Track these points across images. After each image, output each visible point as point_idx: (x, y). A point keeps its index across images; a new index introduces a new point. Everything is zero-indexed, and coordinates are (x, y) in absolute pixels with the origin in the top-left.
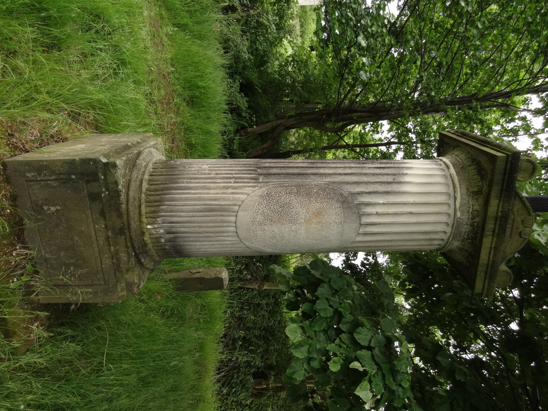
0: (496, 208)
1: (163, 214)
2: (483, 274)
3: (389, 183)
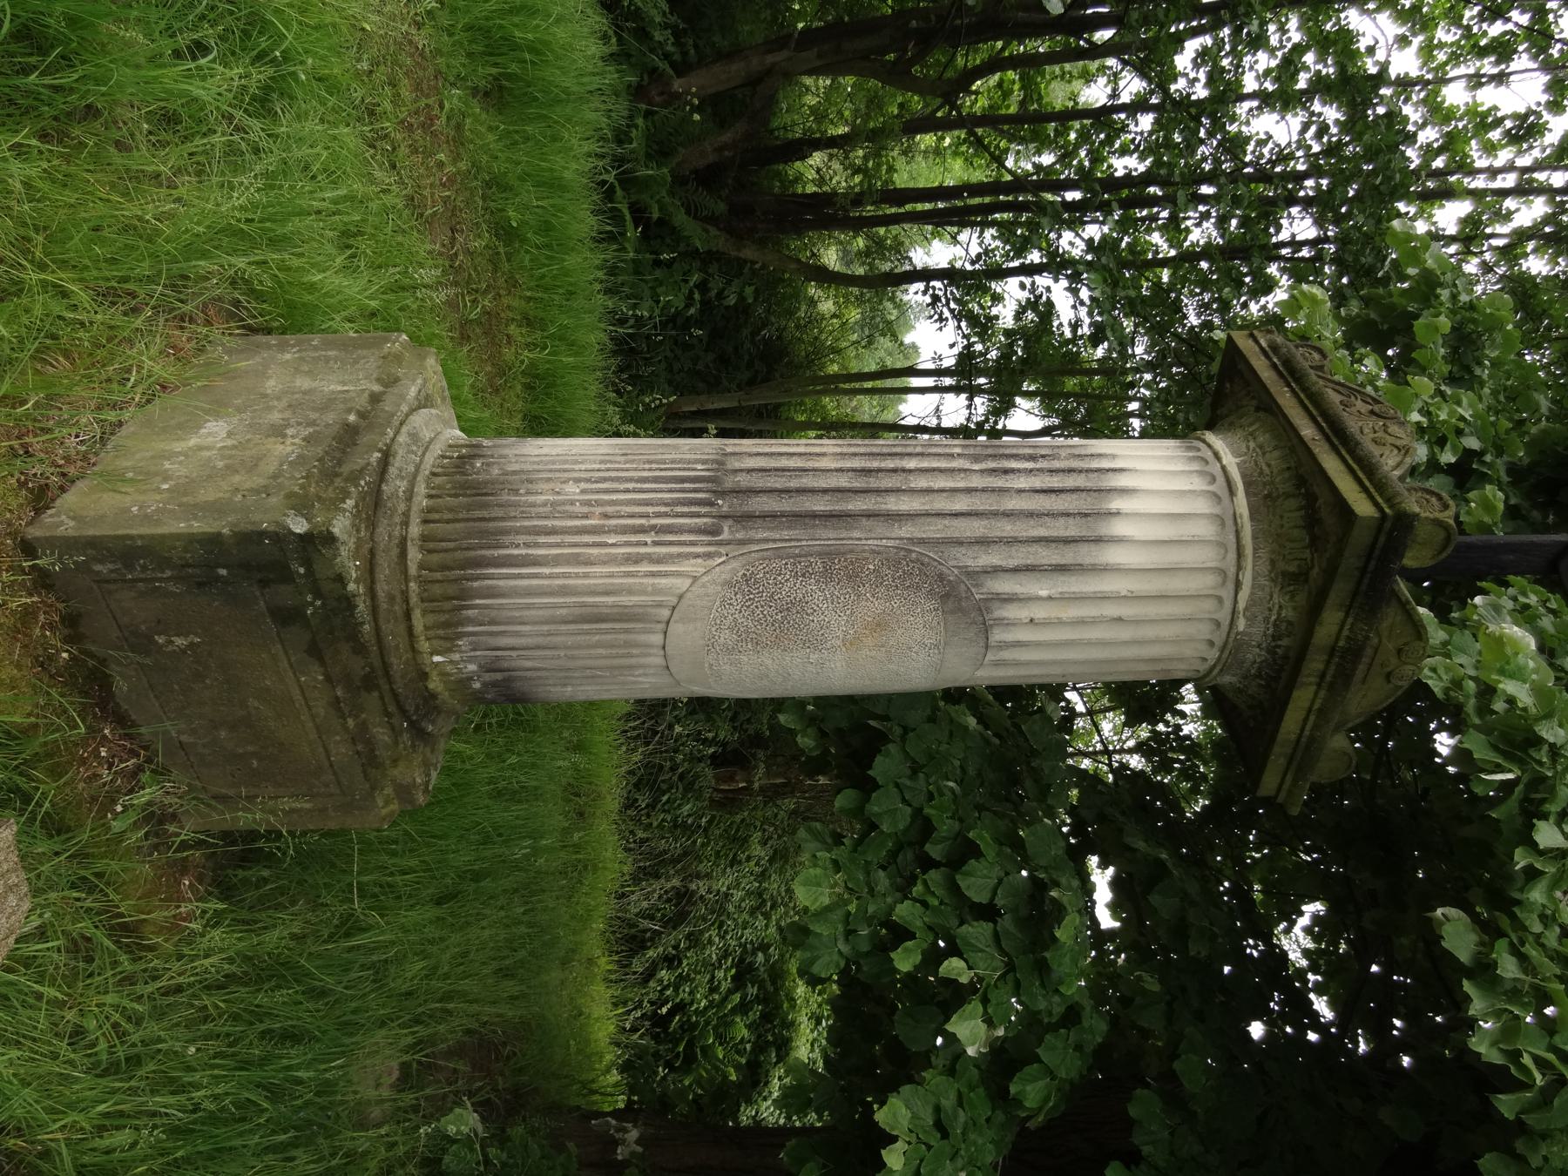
0: (1335, 629)
1: (470, 629)
2: (1282, 761)
3: (1067, 541)
